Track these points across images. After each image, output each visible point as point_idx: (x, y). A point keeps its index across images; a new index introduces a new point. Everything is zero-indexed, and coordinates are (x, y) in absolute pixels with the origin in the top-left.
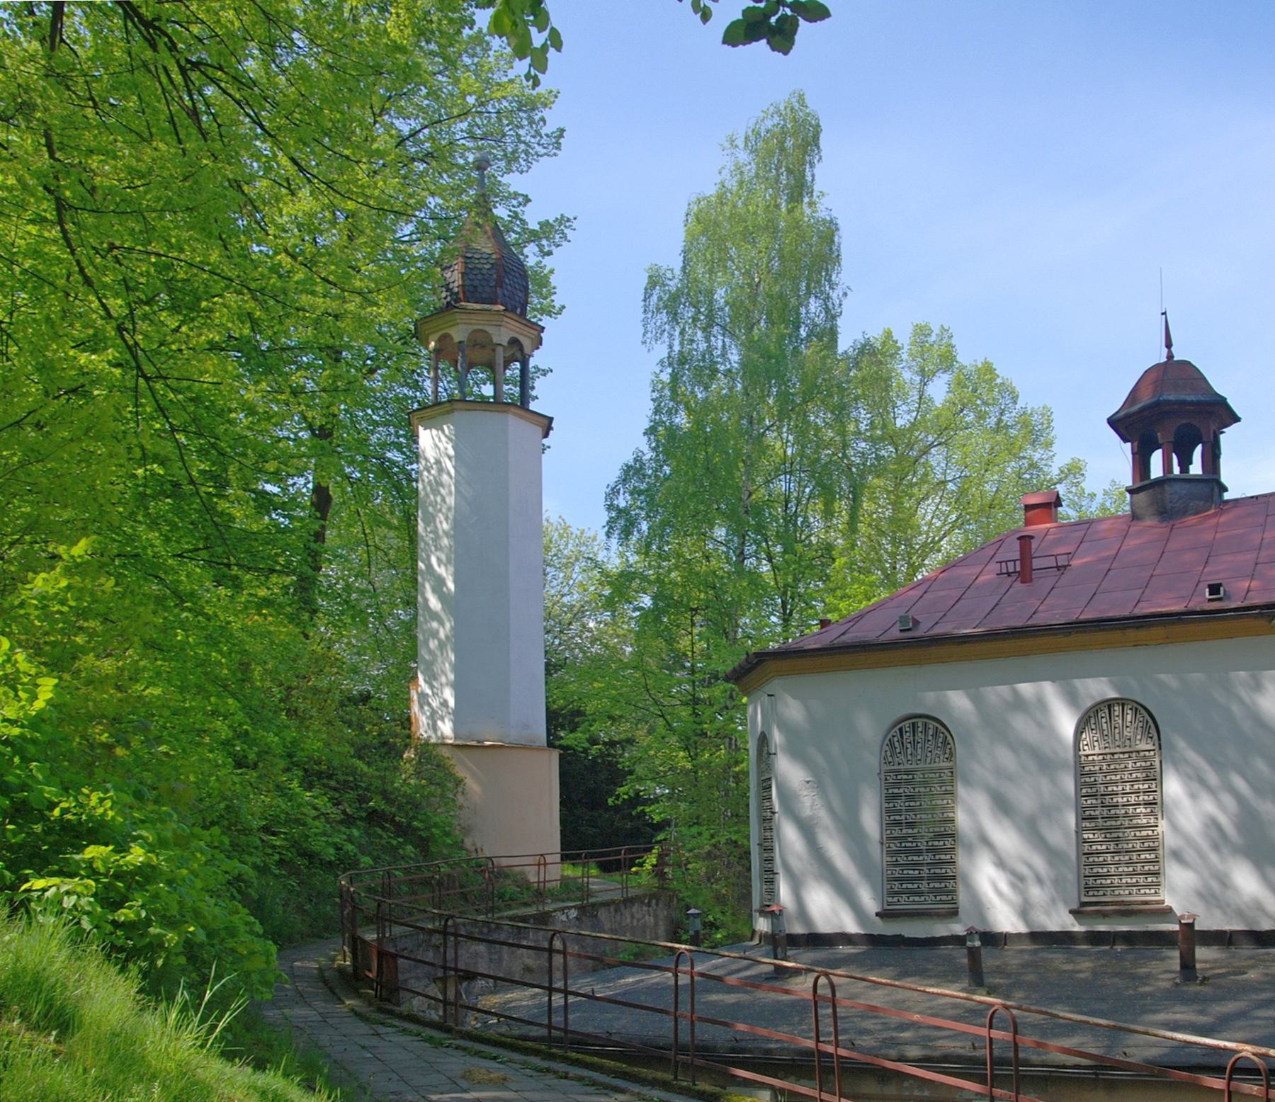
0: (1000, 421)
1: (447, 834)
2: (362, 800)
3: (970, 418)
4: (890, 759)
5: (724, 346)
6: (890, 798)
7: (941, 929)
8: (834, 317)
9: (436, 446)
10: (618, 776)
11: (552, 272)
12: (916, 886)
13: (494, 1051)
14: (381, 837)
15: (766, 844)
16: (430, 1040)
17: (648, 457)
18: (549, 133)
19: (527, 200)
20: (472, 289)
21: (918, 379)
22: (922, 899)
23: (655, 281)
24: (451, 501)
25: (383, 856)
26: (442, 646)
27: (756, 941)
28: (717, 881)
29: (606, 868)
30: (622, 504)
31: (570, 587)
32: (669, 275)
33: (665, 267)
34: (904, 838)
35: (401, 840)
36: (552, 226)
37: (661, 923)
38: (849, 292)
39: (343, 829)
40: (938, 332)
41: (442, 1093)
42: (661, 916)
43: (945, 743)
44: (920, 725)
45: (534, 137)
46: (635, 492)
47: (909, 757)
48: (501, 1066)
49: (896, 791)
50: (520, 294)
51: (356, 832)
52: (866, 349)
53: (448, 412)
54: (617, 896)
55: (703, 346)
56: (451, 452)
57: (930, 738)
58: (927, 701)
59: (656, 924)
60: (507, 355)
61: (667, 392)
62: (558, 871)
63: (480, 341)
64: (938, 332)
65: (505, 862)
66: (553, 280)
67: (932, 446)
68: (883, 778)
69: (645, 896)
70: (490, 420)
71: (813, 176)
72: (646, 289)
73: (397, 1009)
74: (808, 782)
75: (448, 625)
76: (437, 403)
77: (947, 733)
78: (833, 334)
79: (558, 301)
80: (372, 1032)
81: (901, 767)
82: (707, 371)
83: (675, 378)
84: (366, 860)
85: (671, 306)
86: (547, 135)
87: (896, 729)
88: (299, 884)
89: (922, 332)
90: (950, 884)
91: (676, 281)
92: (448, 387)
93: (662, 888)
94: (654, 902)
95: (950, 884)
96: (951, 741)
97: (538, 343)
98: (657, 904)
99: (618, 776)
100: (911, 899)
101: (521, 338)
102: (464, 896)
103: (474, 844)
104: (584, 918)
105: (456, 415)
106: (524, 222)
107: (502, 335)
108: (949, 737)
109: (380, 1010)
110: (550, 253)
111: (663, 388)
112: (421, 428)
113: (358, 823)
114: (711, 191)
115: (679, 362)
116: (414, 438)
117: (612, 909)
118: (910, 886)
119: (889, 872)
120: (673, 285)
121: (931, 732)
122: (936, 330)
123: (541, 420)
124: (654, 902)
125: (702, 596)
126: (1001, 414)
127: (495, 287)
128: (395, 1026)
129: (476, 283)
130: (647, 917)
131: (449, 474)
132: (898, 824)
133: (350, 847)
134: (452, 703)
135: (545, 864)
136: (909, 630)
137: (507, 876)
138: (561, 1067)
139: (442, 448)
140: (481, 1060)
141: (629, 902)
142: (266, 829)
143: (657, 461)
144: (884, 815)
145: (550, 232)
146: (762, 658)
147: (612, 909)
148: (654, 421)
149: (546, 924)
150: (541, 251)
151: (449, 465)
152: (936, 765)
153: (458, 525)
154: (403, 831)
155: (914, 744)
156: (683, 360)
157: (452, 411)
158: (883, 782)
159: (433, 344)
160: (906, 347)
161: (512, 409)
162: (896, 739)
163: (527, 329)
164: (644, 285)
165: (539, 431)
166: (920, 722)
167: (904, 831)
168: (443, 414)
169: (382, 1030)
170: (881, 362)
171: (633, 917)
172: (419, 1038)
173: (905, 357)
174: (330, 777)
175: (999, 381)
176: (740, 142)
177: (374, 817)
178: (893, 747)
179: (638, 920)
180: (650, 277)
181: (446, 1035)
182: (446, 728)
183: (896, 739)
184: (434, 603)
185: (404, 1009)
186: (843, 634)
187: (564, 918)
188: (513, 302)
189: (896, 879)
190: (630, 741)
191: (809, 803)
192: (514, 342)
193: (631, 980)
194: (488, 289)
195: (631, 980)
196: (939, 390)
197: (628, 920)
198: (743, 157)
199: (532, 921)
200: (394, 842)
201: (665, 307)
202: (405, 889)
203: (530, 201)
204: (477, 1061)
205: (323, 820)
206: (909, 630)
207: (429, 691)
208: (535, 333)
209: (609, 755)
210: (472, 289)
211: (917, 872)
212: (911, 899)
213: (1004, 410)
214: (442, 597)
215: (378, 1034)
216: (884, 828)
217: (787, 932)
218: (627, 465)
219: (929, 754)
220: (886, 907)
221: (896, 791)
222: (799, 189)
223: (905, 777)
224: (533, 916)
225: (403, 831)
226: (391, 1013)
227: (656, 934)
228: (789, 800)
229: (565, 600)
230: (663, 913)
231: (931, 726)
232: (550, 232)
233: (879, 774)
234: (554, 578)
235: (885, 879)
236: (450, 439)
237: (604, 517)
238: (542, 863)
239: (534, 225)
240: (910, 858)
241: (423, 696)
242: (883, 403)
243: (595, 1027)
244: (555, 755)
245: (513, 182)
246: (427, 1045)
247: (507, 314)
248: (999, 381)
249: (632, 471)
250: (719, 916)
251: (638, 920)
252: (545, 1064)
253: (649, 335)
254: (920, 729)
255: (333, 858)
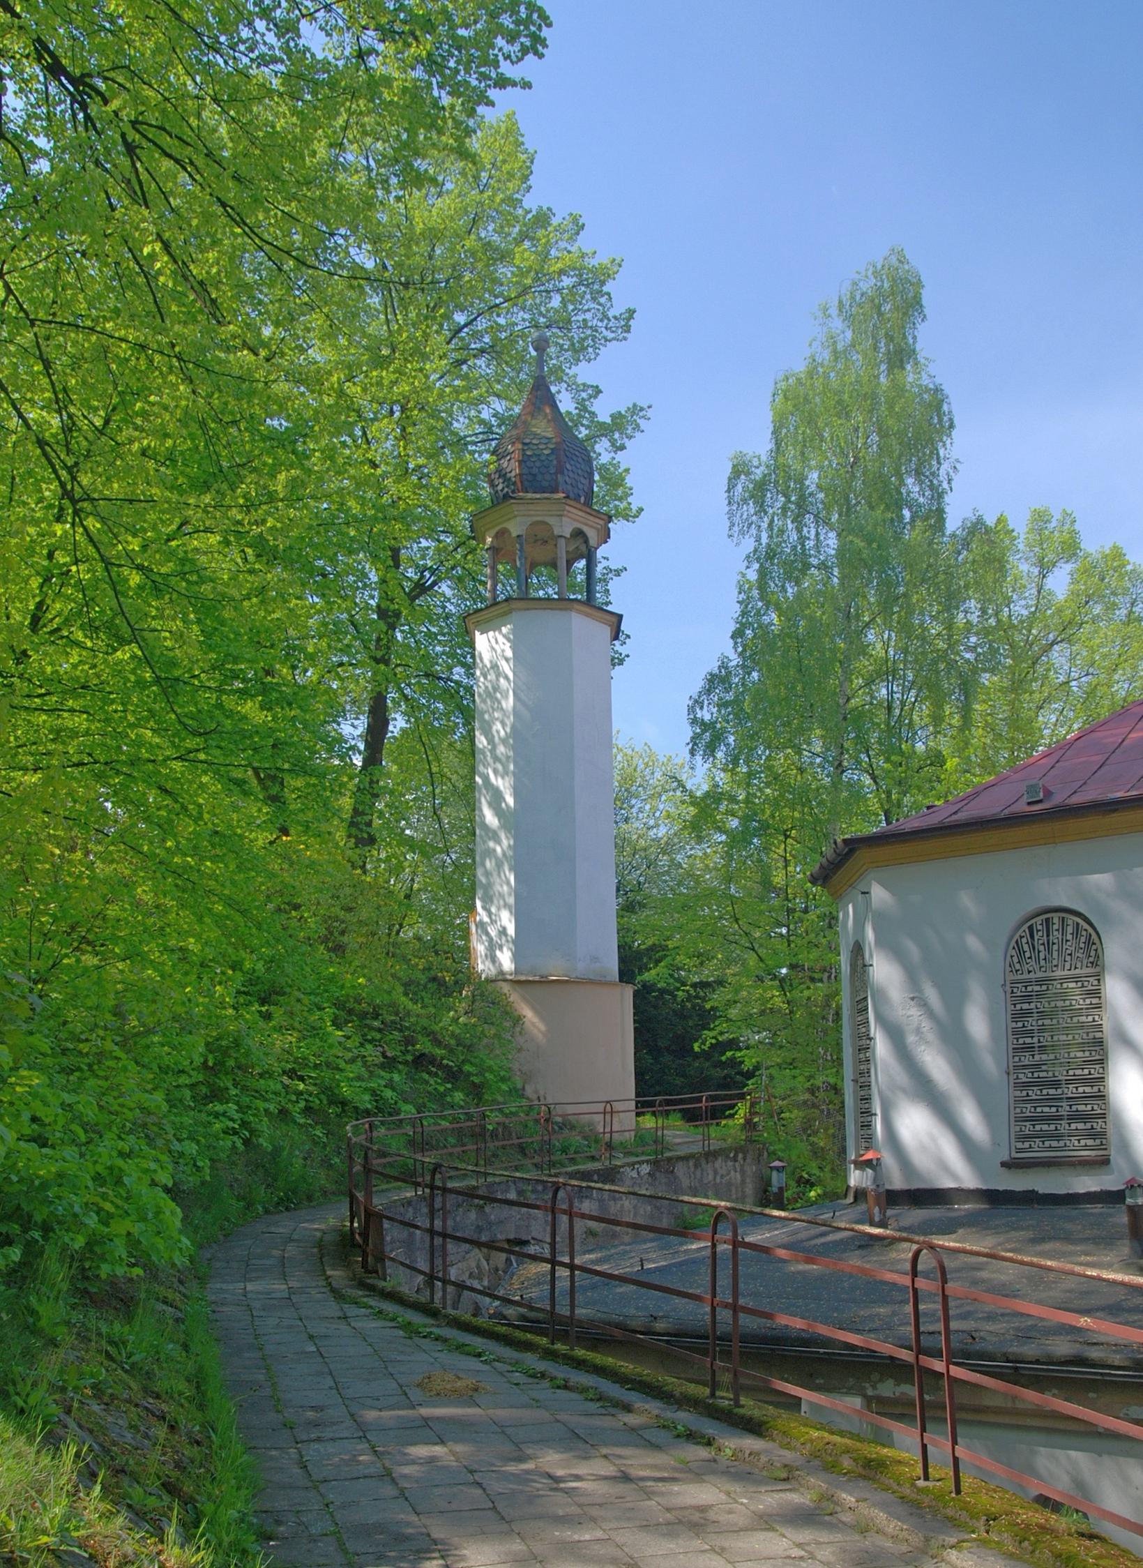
0: (1131, 612)
1: (503, 1080)
2: (409, 1041)
3: (1098, 609)
4: (1018, 967)
5: (817, 534)
6: (1019, 1015)
7: (1086, 1183)
8: (940, 496)
9: (493, 648)
10: (706, 1018)
11: (627, 471)
12: (1052, 1127)
13: (478, 1342)
14: (427, 1082)
15: (862, 1080)
16: (407, 1326)
17: (734, 663)
18: (618, 315)
19: (598, 391)
20: (530, 478)
21: (1036, 571)
22: (1062, 1143)
23: (739, 469)
24: (509, 703)
25: (429, 1104)
26: (499, 866)
27: (850, 1199)
28: (815, 1133)
29: (691, 1117)
30: (707, 717)
31: (657, 819)
32: (756, 463)
33: (751, 454)
34: (1037, 1066)
35: (449, 1086)
36: (624, 417)
37: (748, 1180)
38: (958, 466)
39: (383, 1073)
40: (1059, 517)
41: (380, 1410)
42: (749, 1173)
43: (1089, 942)
44: (1056, 920)
45: (601, 321)
46: (722, 705)
47: (1043, 963)
48: (485, 1367)
49: (1025, 1006)
50: (583, 481)
51: (396, 1077)
52: (976, 528)
53: (505, 614)
54: (696, 1149)
55: (794, 536)
56: (509, 654)
57: (1069, 937)
58: (1059, 893)
59: (743, 1182)
60: (571, 549)
61: (755, 593)
62: (626, 1122)
63: (542, 536)
64: (1059, 517)
65: (570, 1109)
66: (629, 481)
67: (1053, 643)
68: (1008, 989)
69: (730, 1149)
70: (552, 620)
71: (914, 338)
72: (730, 479)
73: (381, 1284)
74: (913, 999)
75: (505, 843)
76: (495, 604)
77: (1090, 930)
78: (938, 516)
79: (635, 502)
80: (340, 1314)
81: (1032, 975)
82: (797, 566)
83: (763, 573)
84: (408, 1110)
85: (758, 493)
86: (615, 318)
87: (1025, 927)
88: (327, 1135)
89: (1040, 519)
90: (1098, 1125)
91: (762, 468)
92: (508, 588)
93: (750, 1140)
94: (740, 1156)
95: (1098, 1125)
96: (1097, 941)
97: (605, 536)
98: (744, 1159)
99: (706, 1018)
100: (1047, 1144)
101: (585, 529)
102: (522, 1149)
103: (536, 1091)
104: (658, 1174)
105: (514, 615)
106: (593, 414)
107: (565, 528)
108: (1094, 936)
109: (362, 1285)
110: (622, 448)
111: (750, 589)
112: (477, 633)
113: (401, 1067)
114: (800, 367)
115: (767, 557)
116: (472, 644)
117: (691, 1163)
118: (1045, 1127)
119: (1018, 1110)
120: (758, 473)
121: (1070, 929)
122: (1057, 516)
123: (608, 617)
124: (740, 1156)
125: (797, 815)
126: (1132, 604)
127: (556, 474)
128: (371, 1307)
129: (535, 471)
130: (732, 1173)
131: (506, 678)
132: (1029, 1048)
133: (388, 1093)
134: (511, 930)
135: (612, 1112)
136: (1040, 801)
137: (573, 1128)
138: (561, 1372)
139: (499, 651)
140: (463, 1357)
141: (711, 1155)
142: (291, 1074)
143: (743, 667)
144: (1011, 1037)
145: (621, 426)
146: (853, 845)
147: (691, 1163)
148: (740, 623)
149: (613, 1182)
150: (613, 445)
151: (506, 668)
152: (1077, 971)
153: (517, 738)
154: (453, 1075)
155: (1048, 945)
156: (771, 554)
157: (510, 612)
158: (1009, 995)
159: (489, 540)
160: (1022, 537)
161: (576, 606)
162: (1024, 940)
163: (592, 518)
164: (728, 474)
165: (607, 632)
166: (1056, 918)
167: (1037, 1058)
168: (498, 616)
169: (352, 1311)
170: (993, 542)
171: (716, 1173)
172: (393, 1324)
173: (1021, 547)
174: (376, 1016)
175: (1129, 568)
176: (834, 311)
177: (421, 1061)
178: (1021, 952)
179: (722, 1177)
180: (734, 466)
181: (430, 1321)
182: (506, 960)
183: (1024, 940)
184: (490, 818)
185: (387, 1285)
186: (955, 813)
187: (634, 1174)
188: (576, 491)
189: (1027, 1119)
190: (721, 983)
191: (909, 1015)
192: (579, 534)
193: (694, 1247)
194: (548, 477)
195: (694, 1247)
196: (1060, 583)
197: (711, 1177)
198: (837, 324)
199: (596, 1177)
200: (442, 1089)
201: (752, 497)
202: (452, 1140)
203: (601, 392)
204: (446, 1358)
205: (360, 1063)
206: (1040, 801)
207: (486, 919)
208: (602, 522)
209: (697, 997)
210: (530, 478)
211: (1054, 1109)
212: (1047, 1144)
213: (1135, 600)
214: (498, 812)
215: (345, 1318)
216: (1011, 1055)
217: (888, 1187)
218: (711, 674)
219: (1068, 958)
220: (1015, 1155)
221: (1025, 1006)
222: (901, 356)
223: (1038, 988)
224: (597, 1172)
225: (453, 1075)
226: (372, 1289)
227: (743, 1192)
228: (880, 995)
229: (651, 833)
230: (751, 1169)
231: (1070, 922)
232: (621, 426)
233: (1004, 985)
234: (641, 810)
235: (1012, 1119)
236: (509, 640)
237: (688, 732)
238: (609, 1111)
239: (604, 417)
240: (1045, 1092)
241: (481, 925)
242: (994, 597)
243: (637, 1308)
244: (629, 991)
245: (584, 372)
246: (401, 1333)
247: (569, 502)
248: (1129, 568)
249: (716, 681)
250: (816, 1171)
251: (722, 1177)
252: (542, 1366)
253: (736, 528)
254: (1056, 927)
255: (369, 1106)
